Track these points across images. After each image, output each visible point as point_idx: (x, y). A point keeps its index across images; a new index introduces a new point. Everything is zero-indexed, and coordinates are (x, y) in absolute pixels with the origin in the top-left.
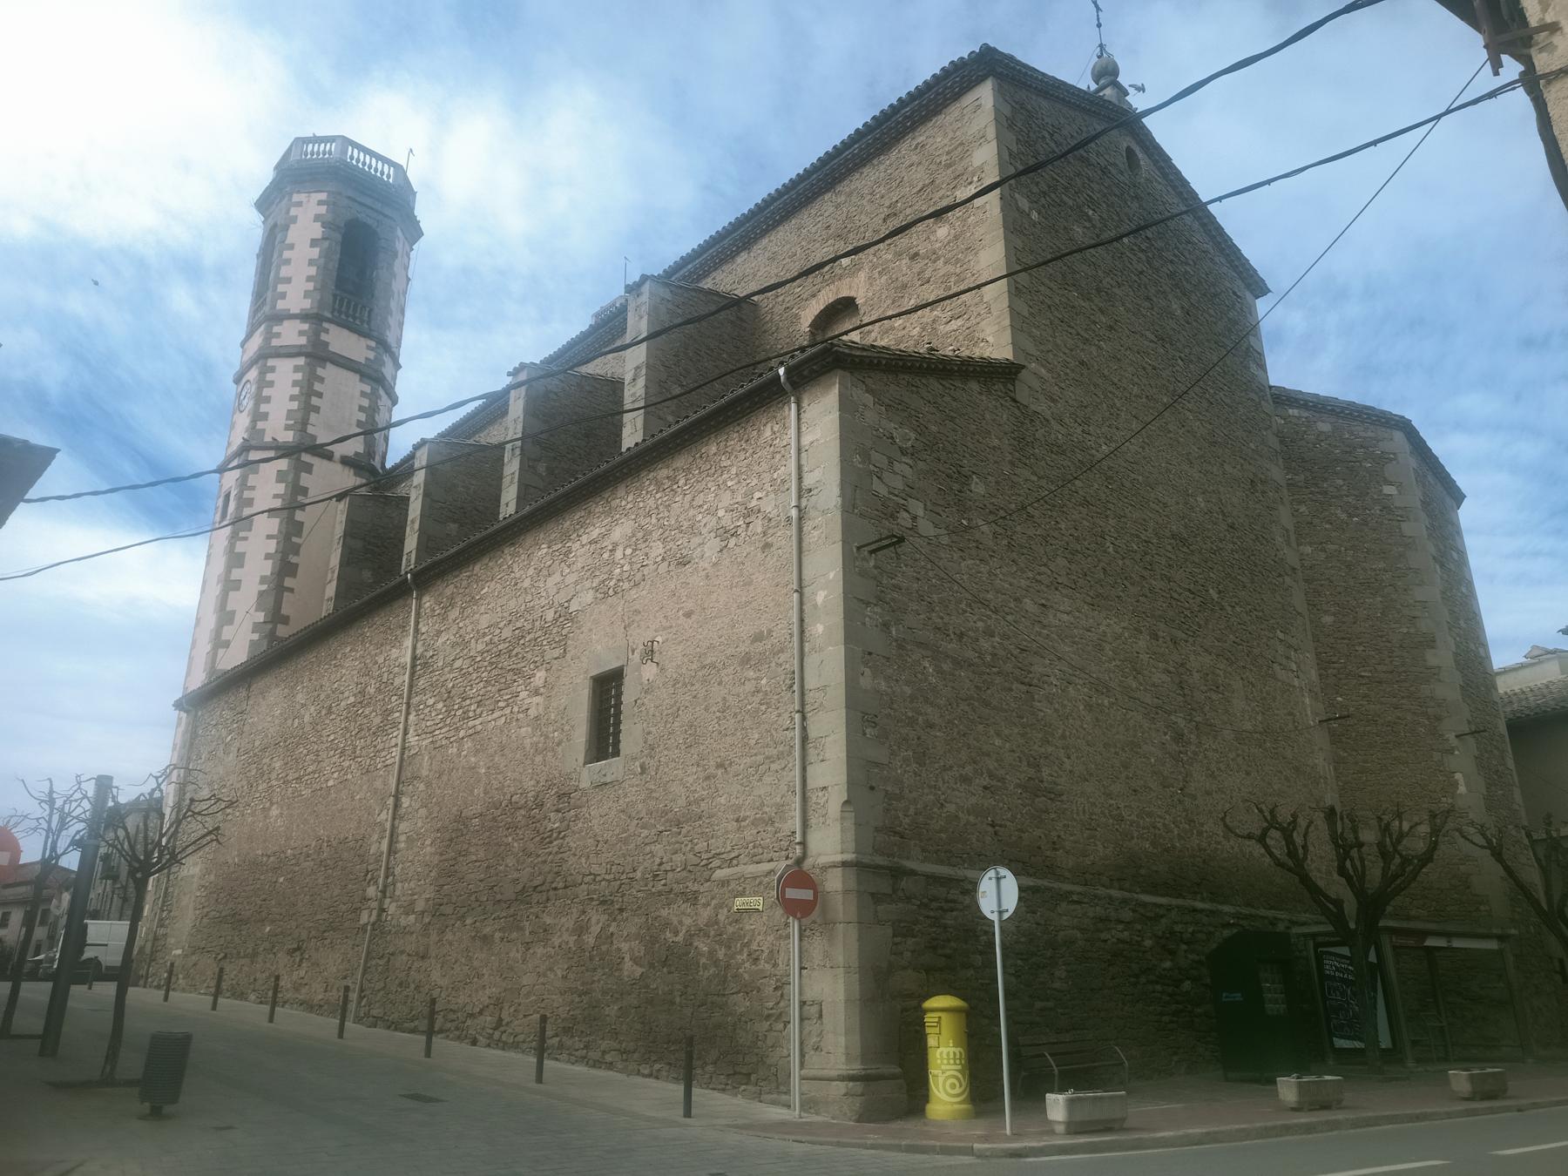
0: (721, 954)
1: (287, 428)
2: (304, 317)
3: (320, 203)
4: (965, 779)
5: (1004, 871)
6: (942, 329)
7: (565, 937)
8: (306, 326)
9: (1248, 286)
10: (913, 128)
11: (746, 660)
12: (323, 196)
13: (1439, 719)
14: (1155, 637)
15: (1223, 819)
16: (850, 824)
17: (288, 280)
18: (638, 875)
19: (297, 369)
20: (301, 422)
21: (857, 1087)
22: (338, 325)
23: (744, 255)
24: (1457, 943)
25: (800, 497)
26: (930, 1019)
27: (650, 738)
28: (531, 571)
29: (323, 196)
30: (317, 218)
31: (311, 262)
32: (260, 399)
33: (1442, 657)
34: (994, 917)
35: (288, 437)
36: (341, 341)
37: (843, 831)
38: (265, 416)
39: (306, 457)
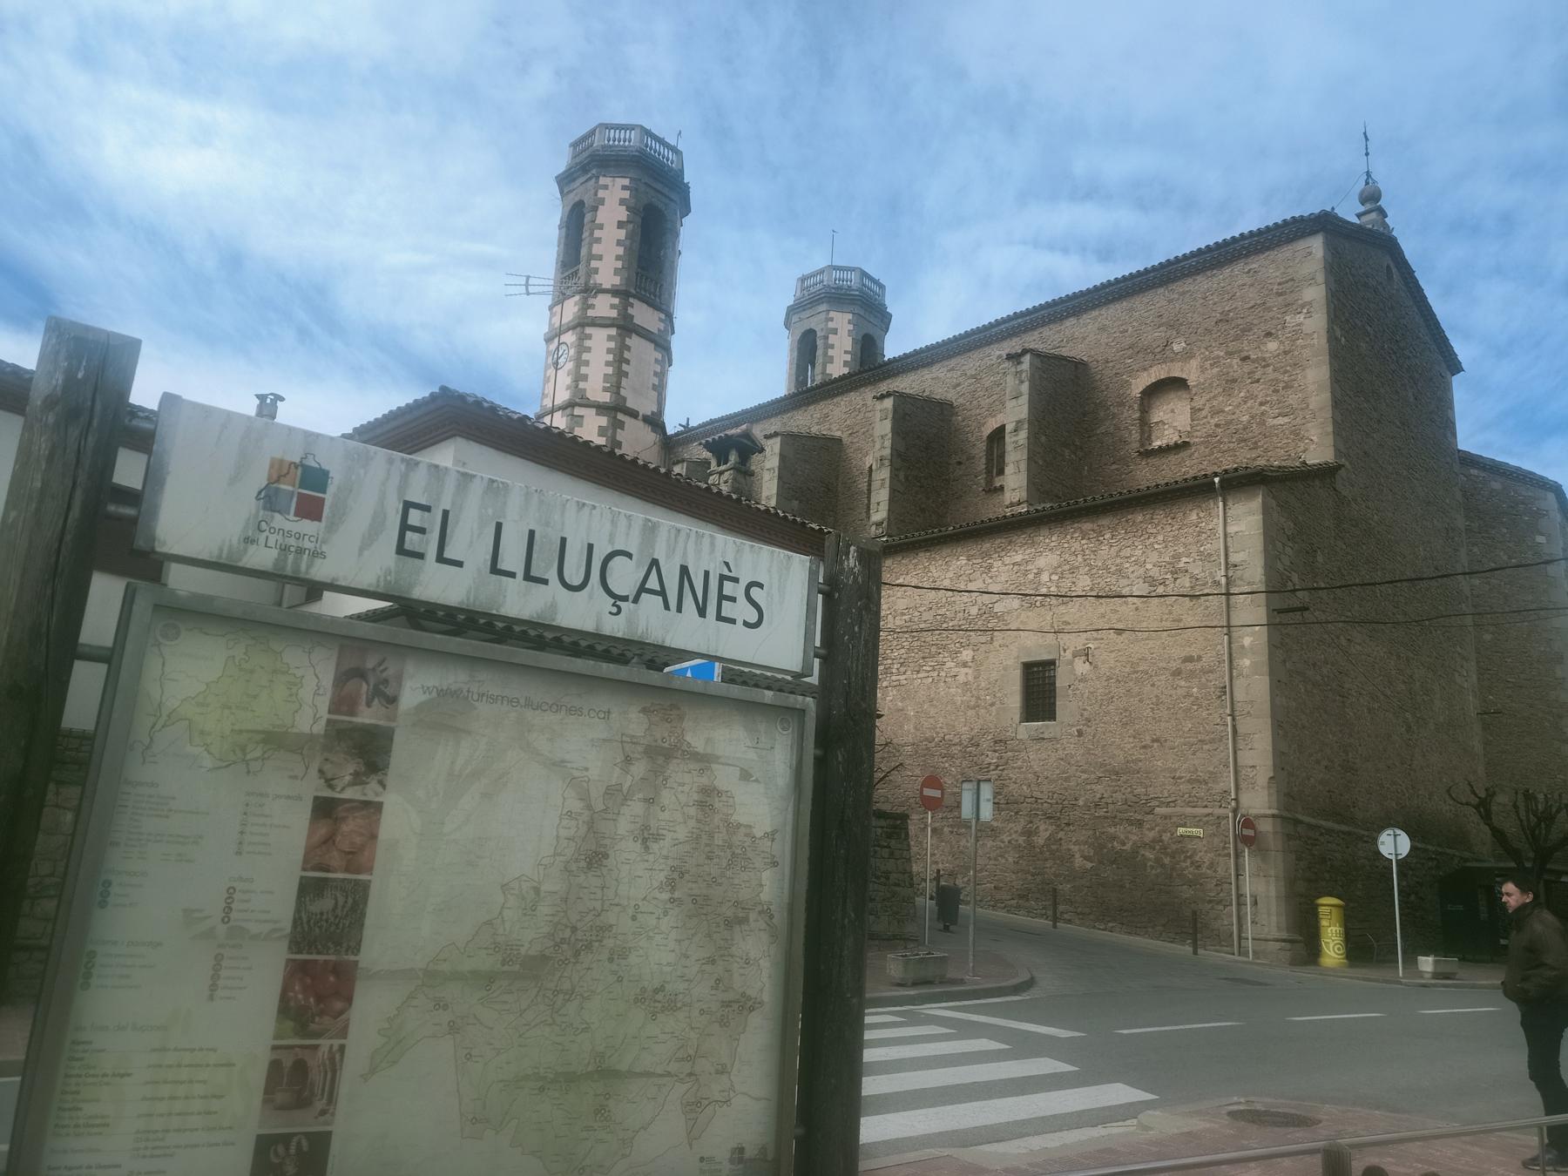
0: (1167, 861)
1: (605, 390)
2: (614, 292)
3: (624, 188)
4: (1318, 762)
5: (1399, 832)
6: (1270, 422)
8: (616, 301)
9: (1449, 367)
10: (1247, 256)
11: (1177, 673)
12: (626, 182)
14: (1399, 657)
17: (600, 258)
18: (1081, 803)
19: (610, 338)
20: (615, 387)
21: (1288, 946)
22: (640, 299)
23: (1073, 321)
25: (1227, 569)
26: (1321, 909)
27: (1086, 714)
28: (950, 574)
29: (626, 182)
30: (622, 202)
31: (619, 243)
32: (580, 362)
34: (1393, 857)
35: (605, 398)
36: (643, 315)
37: (1269, 795)
38: (585, 378)
39: (620, 416)
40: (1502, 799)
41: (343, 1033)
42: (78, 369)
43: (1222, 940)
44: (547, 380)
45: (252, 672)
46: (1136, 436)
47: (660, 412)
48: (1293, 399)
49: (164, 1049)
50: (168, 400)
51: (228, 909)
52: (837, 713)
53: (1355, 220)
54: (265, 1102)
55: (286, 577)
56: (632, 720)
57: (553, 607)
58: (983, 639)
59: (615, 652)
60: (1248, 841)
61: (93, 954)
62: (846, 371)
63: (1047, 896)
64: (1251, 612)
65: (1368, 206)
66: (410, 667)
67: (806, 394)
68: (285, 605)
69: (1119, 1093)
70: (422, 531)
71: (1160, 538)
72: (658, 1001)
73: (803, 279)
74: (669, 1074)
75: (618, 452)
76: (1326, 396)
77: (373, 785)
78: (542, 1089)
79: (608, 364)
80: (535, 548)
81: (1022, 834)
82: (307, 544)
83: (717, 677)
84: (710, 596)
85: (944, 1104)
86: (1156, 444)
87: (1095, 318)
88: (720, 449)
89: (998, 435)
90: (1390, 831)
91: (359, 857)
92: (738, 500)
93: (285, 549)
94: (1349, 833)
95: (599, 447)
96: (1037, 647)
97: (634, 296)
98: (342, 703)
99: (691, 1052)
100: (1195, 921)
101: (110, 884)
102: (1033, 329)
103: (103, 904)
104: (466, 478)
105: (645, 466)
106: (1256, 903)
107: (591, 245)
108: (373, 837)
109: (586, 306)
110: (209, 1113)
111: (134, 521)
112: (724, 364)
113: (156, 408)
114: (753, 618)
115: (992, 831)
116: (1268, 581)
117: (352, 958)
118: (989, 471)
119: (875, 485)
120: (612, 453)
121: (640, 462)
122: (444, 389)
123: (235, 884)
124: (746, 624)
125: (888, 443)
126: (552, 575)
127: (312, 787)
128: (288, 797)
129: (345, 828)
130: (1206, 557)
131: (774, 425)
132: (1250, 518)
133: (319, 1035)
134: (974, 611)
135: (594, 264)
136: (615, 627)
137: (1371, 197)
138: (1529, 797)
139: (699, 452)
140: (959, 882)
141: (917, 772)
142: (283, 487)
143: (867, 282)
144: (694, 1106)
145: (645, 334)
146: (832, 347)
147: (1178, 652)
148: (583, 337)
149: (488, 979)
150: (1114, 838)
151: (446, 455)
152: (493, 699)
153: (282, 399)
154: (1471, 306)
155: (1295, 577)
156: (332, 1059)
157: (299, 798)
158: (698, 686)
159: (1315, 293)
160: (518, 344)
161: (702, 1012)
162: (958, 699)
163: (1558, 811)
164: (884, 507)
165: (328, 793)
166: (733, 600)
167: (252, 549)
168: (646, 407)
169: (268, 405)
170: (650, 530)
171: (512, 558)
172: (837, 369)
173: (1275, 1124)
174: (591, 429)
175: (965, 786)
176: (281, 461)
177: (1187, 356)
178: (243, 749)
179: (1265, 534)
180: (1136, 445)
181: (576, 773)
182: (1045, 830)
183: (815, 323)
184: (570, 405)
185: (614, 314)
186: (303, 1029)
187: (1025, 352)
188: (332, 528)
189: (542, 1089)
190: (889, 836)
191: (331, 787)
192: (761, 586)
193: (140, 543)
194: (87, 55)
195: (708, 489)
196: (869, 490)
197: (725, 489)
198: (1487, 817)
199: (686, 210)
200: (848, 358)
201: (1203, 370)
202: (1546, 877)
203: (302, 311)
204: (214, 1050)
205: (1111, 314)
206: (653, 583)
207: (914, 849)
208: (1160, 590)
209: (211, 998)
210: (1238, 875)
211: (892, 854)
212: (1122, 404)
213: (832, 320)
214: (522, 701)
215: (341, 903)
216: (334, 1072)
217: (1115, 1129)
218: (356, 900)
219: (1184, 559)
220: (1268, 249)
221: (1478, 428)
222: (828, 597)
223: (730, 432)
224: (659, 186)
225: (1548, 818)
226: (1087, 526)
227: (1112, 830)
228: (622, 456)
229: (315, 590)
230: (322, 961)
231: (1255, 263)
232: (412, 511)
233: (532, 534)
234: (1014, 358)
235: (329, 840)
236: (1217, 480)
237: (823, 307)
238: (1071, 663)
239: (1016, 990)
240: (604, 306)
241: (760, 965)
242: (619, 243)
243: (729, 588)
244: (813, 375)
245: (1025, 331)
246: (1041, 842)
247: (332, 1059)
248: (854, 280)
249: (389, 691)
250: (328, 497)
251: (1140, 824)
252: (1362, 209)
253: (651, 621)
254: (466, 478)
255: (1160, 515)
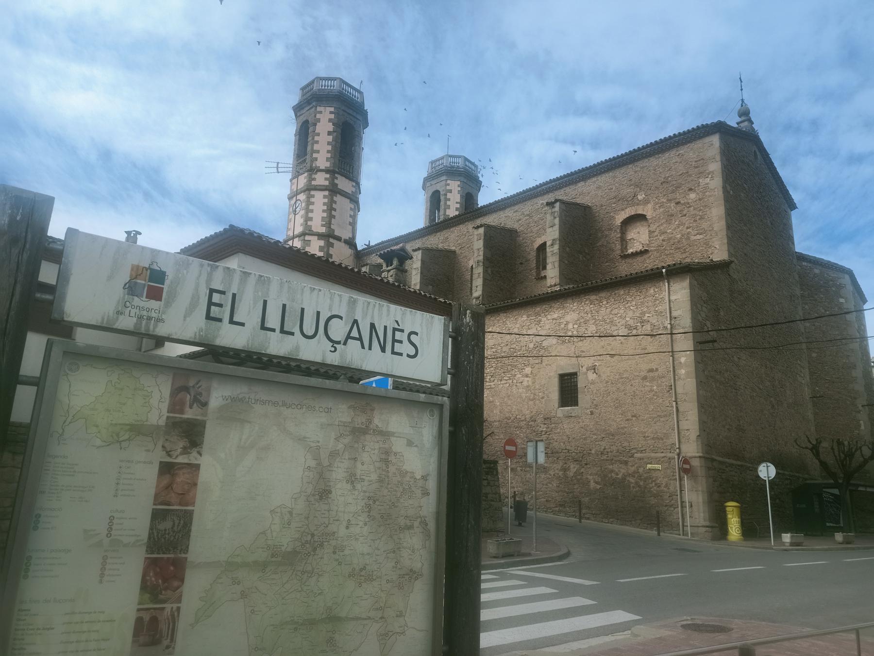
0: (642, 483)
1: (323, 225)
2: (327, 171)
3: (331, 113)
5: (769, 464)
6: (693, 238)
7: (557, 471)
8: (328, 176)
9: (789, 206)
10: (678, 146)
11: (645, 378)
12: (332, 109)
13: (855, 398)
15: (795, 441)
16: (699, 443)
17: (318, 152)
18: (593, 452)
19: (325, 197)
21: (710, 529)
22: (342, 175)
23: (582, 183)
24: (869, 490)
26: (728, 509)
29: (332, 109)
30: (330, 120)
31: (329, 143)
32: (308, 211)
33: (857, 373)
34: (766, 479)
35: (323, 230)
36: (343, 183)
38: (311, 219)
39: (331, 240)
40: (825, 444)
41: (179, 600)
42: (17, 214)
43: (673, 527)
44: (289, 221)
45: (122, 389)
46: (619, 247)
47: (354, 238)
48: (705, 225)
49: (73, 613)
50: (71, 232)
51: (110, 529)
52: (461, 406)
53: (736, 126)
54: (133, 642)
55: (141, 334)
56: (343, 412)
57: (297, 348)
58: (537, 361)
59: (331, 373)
60: (686, 471)
61: (29, 558)
62: (457, 213)
63: (576, 505)
64: (685, 344)
65: (743, 118)
66: (215, 384)
67: (435, 227)
68: (143, 350)
69: (620, 616)
70: (220, 305)
71: (634, 303)
72: (362, 575)
73: (432, 162)
74: (369, 618)
75: (331, 260)
76: (723, 223)
77: (194, 454)
78: (296, 629)
79: (324, 211)
80: (287, 314)
81: (561, 470)
82: (153, 315)
83: (390, 387)
84: (387, 340)
85: (522, 625)
86: (630, 251)
87: (594, 182)
88: (388, 258)
89: (543, 247)
90: (764, 464)
91: (187, 496)
92: (399, 286)
93: (140, 318)
94: (742, 466)
95: (320, 258)
96: (566, 365)
97: (338, 173)
98: (176, 406)
99: (382, 605)
100: (658, 517)
101: (40, 516)
102: (560, 188)
103: (36, 528)
104: (246, 274)
105: (346, 267)
106: (691, 506)
107: (313, 145)
108: (195, 484)
109: (311, 179)
110: (99, 650)
111: (51, 303)
112: (389, 210)
113: (62, 237)
114: (413, 352)
115: (545, 469)
116: (694, 327)
117: (183, 555)
118: (538, 268)
119: (475, 276)
120: (327, 260)
121: (343, 266)
122: (231, 226)
123: (114, 514)
124: (408, 356)
125: (481, 253)
126: (296, 330)
127: (159, 456)
128: (145, 462)
129: (178, 480)
130: (659, 314)
131: (418, 244)
132: (683, 291)
133: (164, 602)
134: (531, 346)
135: (315, 155)
136: (333, 359)
137: (745, 113)
138: (840, 443)
139: (376, 260)
140: (527, 498)
141: (502, 436)
142: (139, 281)
143: (467, 163)
144: (384, 637)
145: (344, 194)
146: (449, 200)
147: (645, 367)
148: (309, 197)
149: (261, 566)
150: (612, 471)
151: (234, 263)
152: (264, 403)
153: (140, 234)
154: (800, 173)
155: (708, 324)
156: (173, 616)
157: (151, 463)
158: (382, 392)
159: (715, 166)
160: (271, 199)
161: (388, 581)
162: (524, 395)
163: (856, 451)
164: (480, 289)
165: (168, 460)
166: (401, 342)
167: (121, 317)
168: (346, 235)
169: (132, 236)
170: (352, 303)
171: (273, 320)
172: (452, 212)
173: (707, 631)
174: (315, 247)
175: (529, 444)
176: (138, 266)
177: (646, 202)
178: (118, 435)
179: (691, 300)
180: (619, 252)
181: (313, 445)
182: (573, 468)
183: (440, 187)
184: (303, 234)
185: (327, 183)
186: (155, 599)
187: (556, 201)
188: (168, 305)
189: (296, 629)
190: (487, 473)
191: (170, 456)
192: (416, 334)
193: (55, 316)
194: (20, 39)
195: (382, 280)
196: (472, 279)
197: (391, 280)
198: (817, 455)
199: (366, 125)
200: (458, 206)
201: (655, 210)
202: (851, 488)
203: (145, 182)
204: (103, 612)
205: (603, 180)
206: (355, 333)
207: (501, 480)
208: (634, 332)
209: (101, 582)
210: (681, 491)
211: (488, 483)
212: (611, 229)
213: (449, 185)
214: (280, 404)
215: (176, 524)
216: (174, 623)
217: (620, 636)
218: (186, 519)
219: (647, 315)
220: (689, 142)
221: (805, 240)
222: (455, 339)
223: (393, 248)
224: (351, 112)
225: (850, 455)
226: (593, 297)
227: (611, 467)
228: (333, 262)
229: (160, 341)
230: (166, 557)
231: (682, 150)
232: (214, 294)
233: (284, 306)
234: (550, 204)
235: (169, 487)
236: (664, 270)
237: (444, 178)
238: (586, 374)
239: (560, 558)
240: (321, 179)
241: (419, 551)
242: (329, 143)
243: (398, 335)
244: (439, 216)
245: (556, 190)
246: (571, 474)
247: (173, 616)
248: (460, 163)
249: (202, 399)
250: (165, 287)
251: (626, 463)
252: (739, 120)
253: (354, 355)
254: (246, 274)
255: (633, 290)
